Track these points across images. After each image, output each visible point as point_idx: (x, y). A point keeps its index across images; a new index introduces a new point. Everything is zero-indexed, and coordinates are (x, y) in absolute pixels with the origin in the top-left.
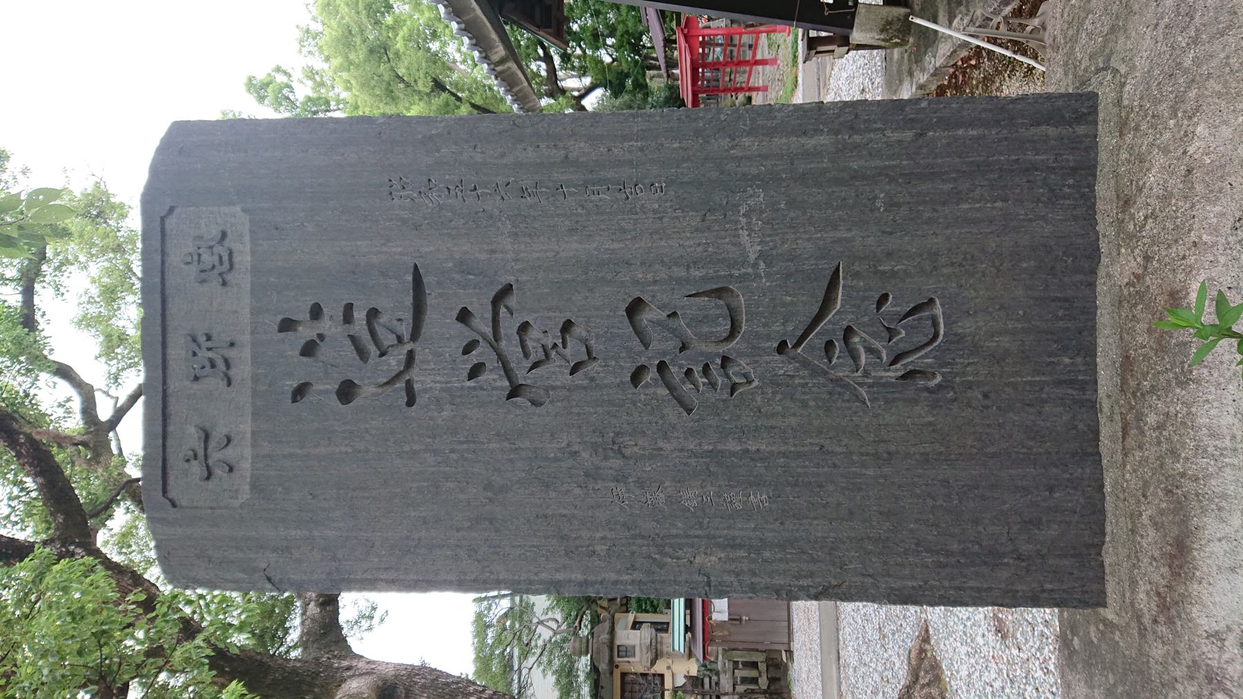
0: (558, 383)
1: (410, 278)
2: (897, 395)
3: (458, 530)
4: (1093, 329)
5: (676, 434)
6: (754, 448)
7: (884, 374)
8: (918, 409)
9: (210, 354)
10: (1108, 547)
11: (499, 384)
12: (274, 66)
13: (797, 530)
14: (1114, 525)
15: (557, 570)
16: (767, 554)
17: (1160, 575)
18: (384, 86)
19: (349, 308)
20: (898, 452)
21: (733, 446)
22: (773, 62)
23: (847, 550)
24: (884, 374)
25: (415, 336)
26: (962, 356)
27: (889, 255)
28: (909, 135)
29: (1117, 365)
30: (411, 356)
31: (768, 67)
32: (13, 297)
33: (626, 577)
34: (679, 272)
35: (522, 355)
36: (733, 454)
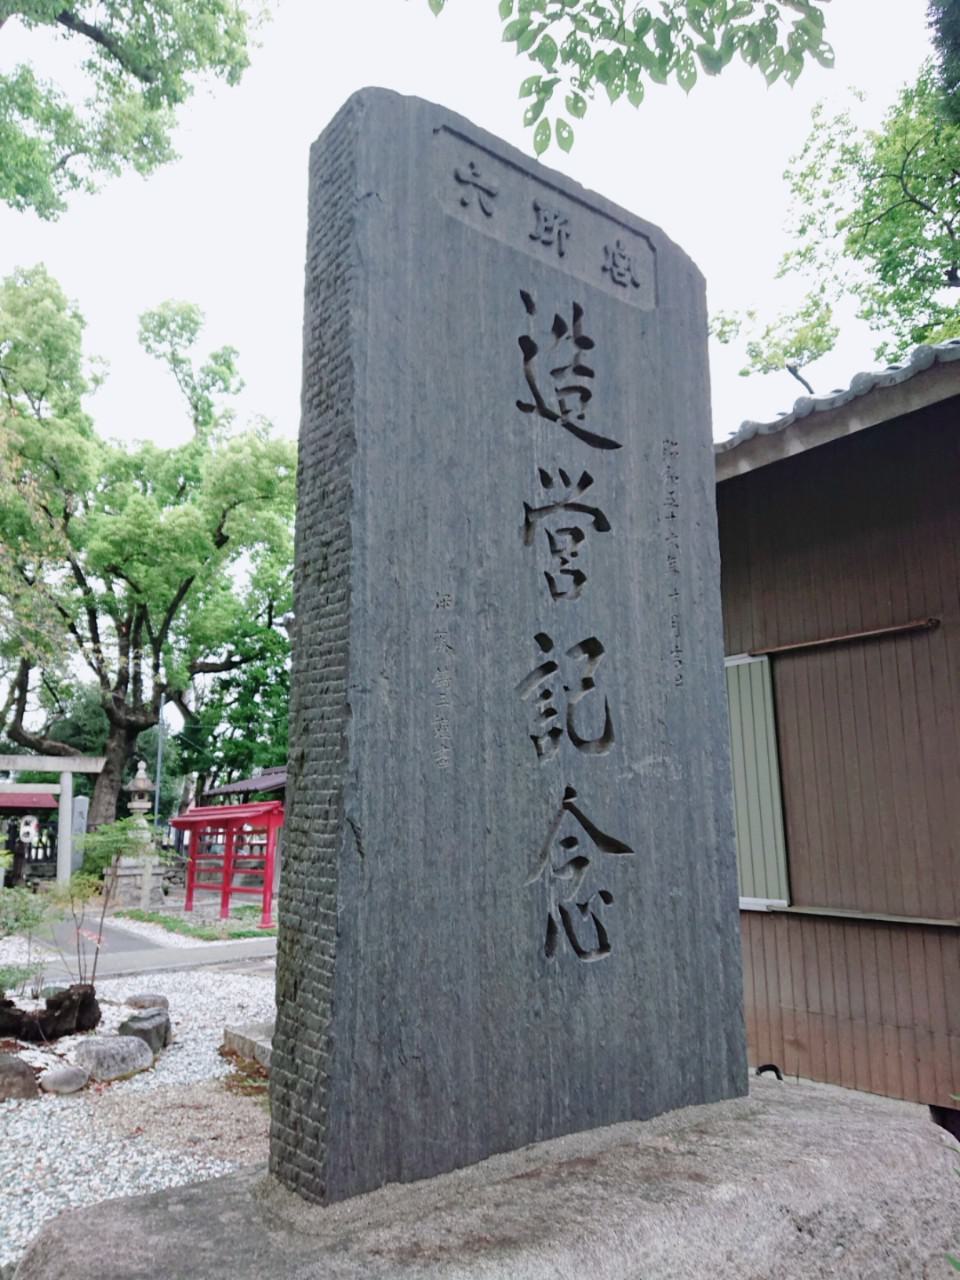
0: (538, 558)
1: (613, 438)
2: (536, 915)
3: (413, 417)
4: (591, 1126)
5: (497, 673)
6: (486, 757)
7: (552, 900)
8: (524, 938)
9: (556, 231)
10: (402, 1189)
11: (536, 498)
12: (245, 381)
13: (415, 800)
14: (428, 1189)
15: (376, 517)
16: (391, 762)
17: (902, 1052)
18: (233, 487)
19: (589, 373)
20: (486, 917)
21: (489, 733)
22: (224, 913)
23: (396, 859)
24: (552, 900)
25: (569, 426)
26: (568, 984)
27: (640, 902)
28: (718, 917)
29: (577, 1155)
30: (553, 417)
31: (219, 908)
32: (93, 14)
33: (369, 594)
34: (623, 692)
35: (560, 527)
36: (481, 733)
